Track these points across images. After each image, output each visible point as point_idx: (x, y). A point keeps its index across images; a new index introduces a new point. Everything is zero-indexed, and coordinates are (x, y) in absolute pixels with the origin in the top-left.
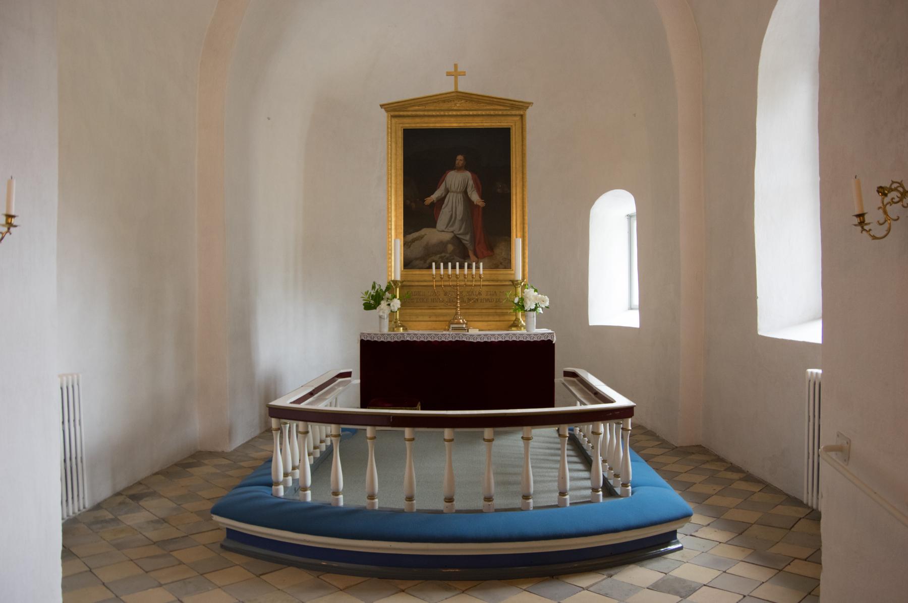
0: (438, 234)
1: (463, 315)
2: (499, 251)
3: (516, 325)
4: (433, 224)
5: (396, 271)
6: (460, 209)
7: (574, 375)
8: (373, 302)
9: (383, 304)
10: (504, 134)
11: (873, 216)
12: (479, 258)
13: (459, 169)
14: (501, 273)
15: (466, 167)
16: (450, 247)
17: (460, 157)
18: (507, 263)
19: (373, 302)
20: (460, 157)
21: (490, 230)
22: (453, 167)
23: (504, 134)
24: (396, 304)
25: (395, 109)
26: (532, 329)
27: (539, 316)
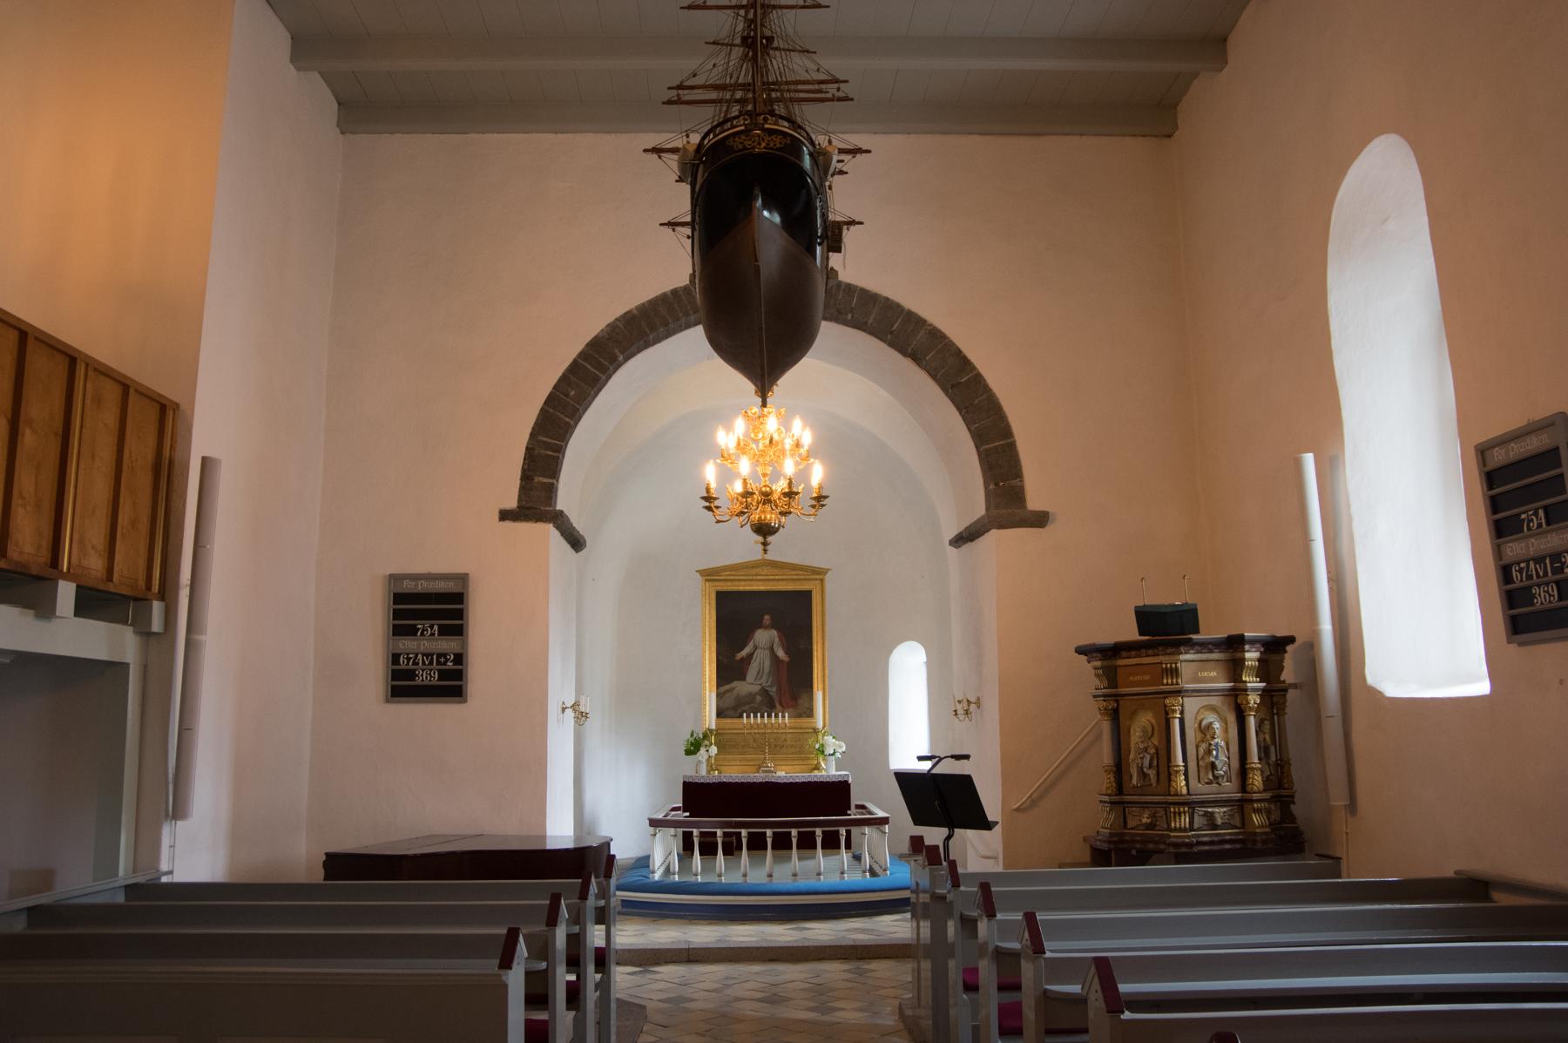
0: (746, 687)
1: (772, 760)
2: (803, 701)
3: (817, 768)
4: (743, 678)
5: (710, 720)
6: (767, 664)
7: (863, 807)
8: (693, 748)
9: (703, 750)
10: (807, 595)
11: (960, 711)
12: (784, 708)
13: (766, 628)
14: (804, 721)
15: (773, 626)
16: (759, 698)
17: (767, 617)
18: (810, 713)
19: (693, 748)
20: (767, 617)
21: (794, 683)
22: (760, 626)
23: (807, 595)
24: (714, 750)
25: (709, 575)
26: (830, 771)
27: (837, 760)
